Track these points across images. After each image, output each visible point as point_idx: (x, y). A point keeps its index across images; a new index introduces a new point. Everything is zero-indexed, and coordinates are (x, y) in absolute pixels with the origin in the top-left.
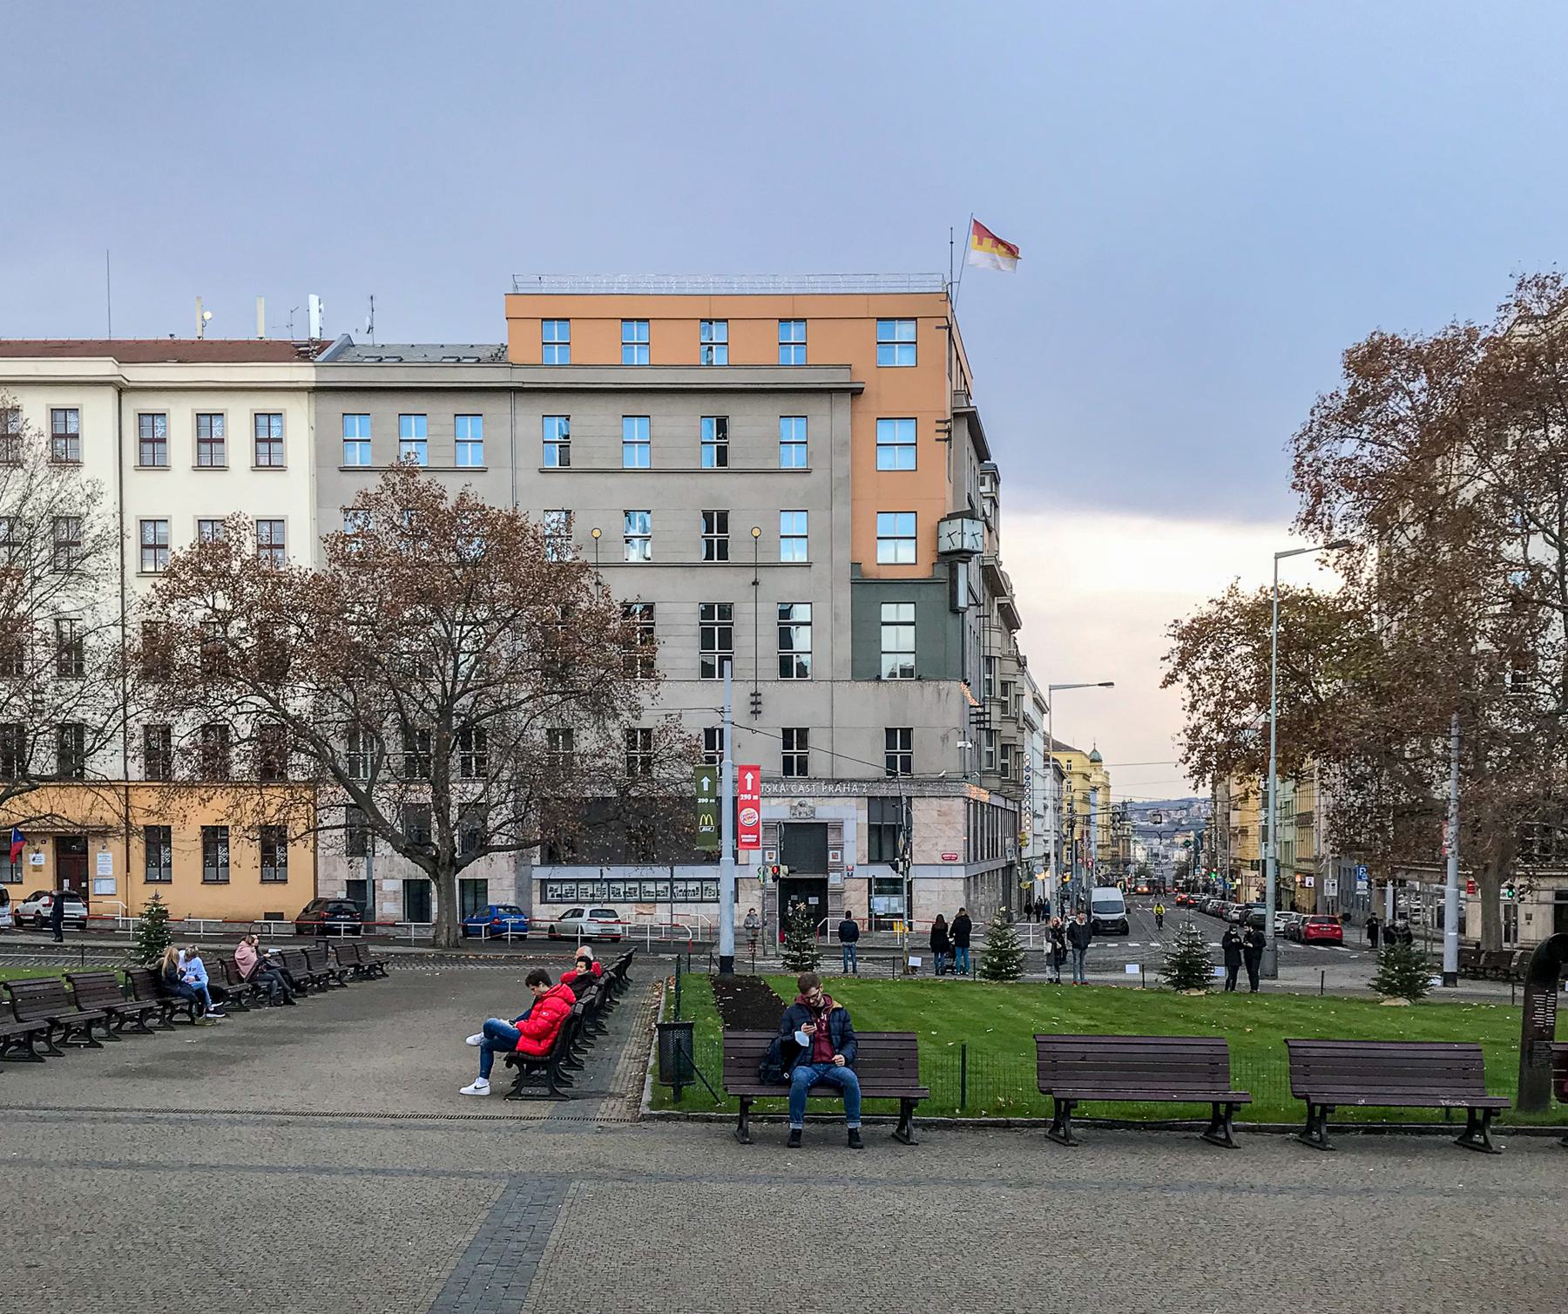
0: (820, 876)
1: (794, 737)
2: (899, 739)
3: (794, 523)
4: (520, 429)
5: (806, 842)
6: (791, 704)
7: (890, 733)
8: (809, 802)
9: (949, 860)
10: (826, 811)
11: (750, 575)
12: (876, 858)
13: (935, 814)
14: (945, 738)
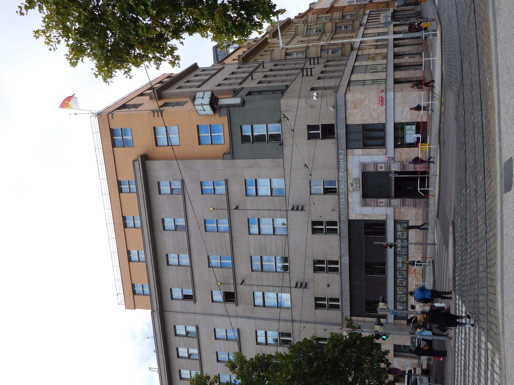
4: (178, 310)
5: (374, 185)
8: (350, 181)
9: (382, 101)
10: (355, 173)
12: (381, 144)
14: (312, 107)
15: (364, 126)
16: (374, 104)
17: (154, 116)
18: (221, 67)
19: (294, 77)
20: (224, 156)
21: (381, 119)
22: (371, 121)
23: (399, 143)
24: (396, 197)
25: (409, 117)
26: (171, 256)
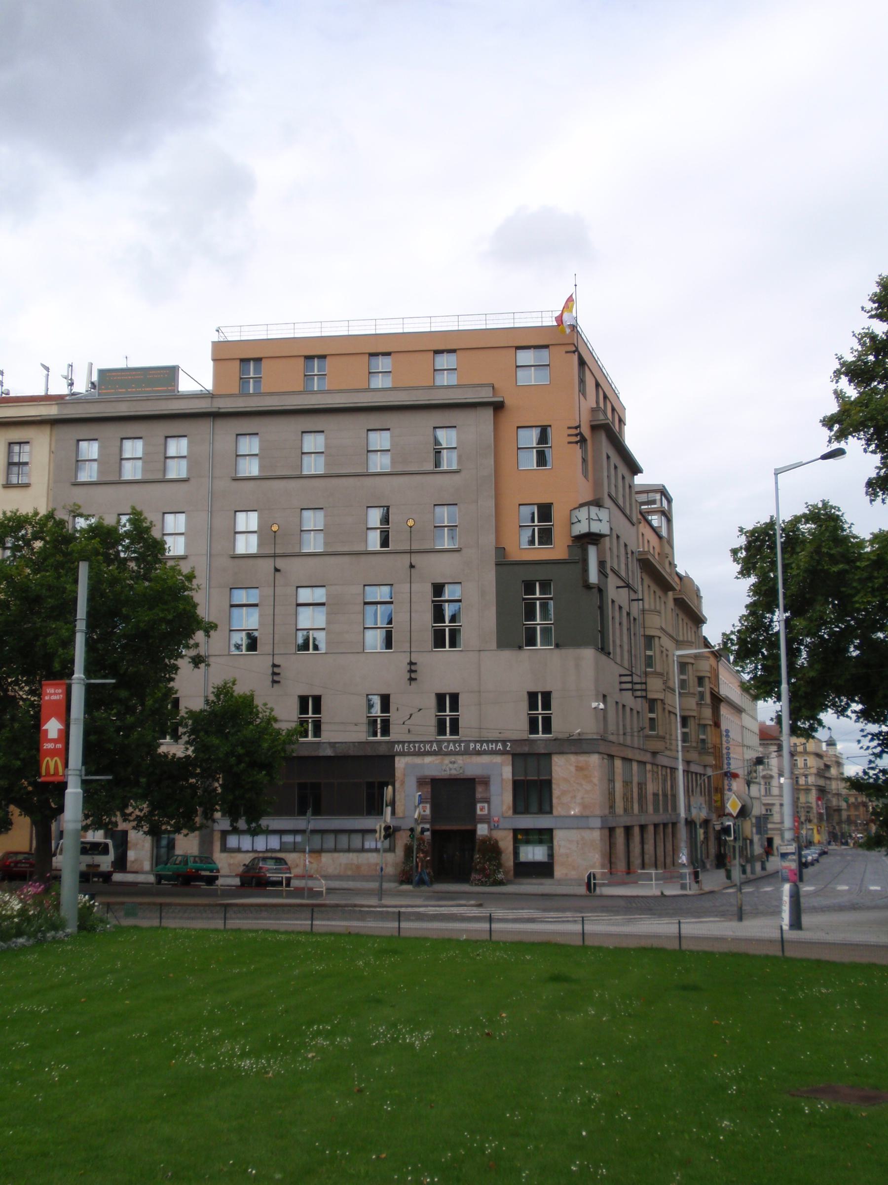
0: (469, 827)
1: (448, 701)
2: (538, 700)
3: (312, 520)
6: (445, 670)
7: (532, 696)
11: (405, 560)
13: (573, 769)
15: (548, 783)
16: (582, 798)
17: (569, 428)
18: (634, 520)
19: (618, 660)
20: (500, 551)
21: (559, 809)
22: (556, 792)
23: (520, 837)
24: (434, 833)
25: (562, 851)
26: (320, 438)
